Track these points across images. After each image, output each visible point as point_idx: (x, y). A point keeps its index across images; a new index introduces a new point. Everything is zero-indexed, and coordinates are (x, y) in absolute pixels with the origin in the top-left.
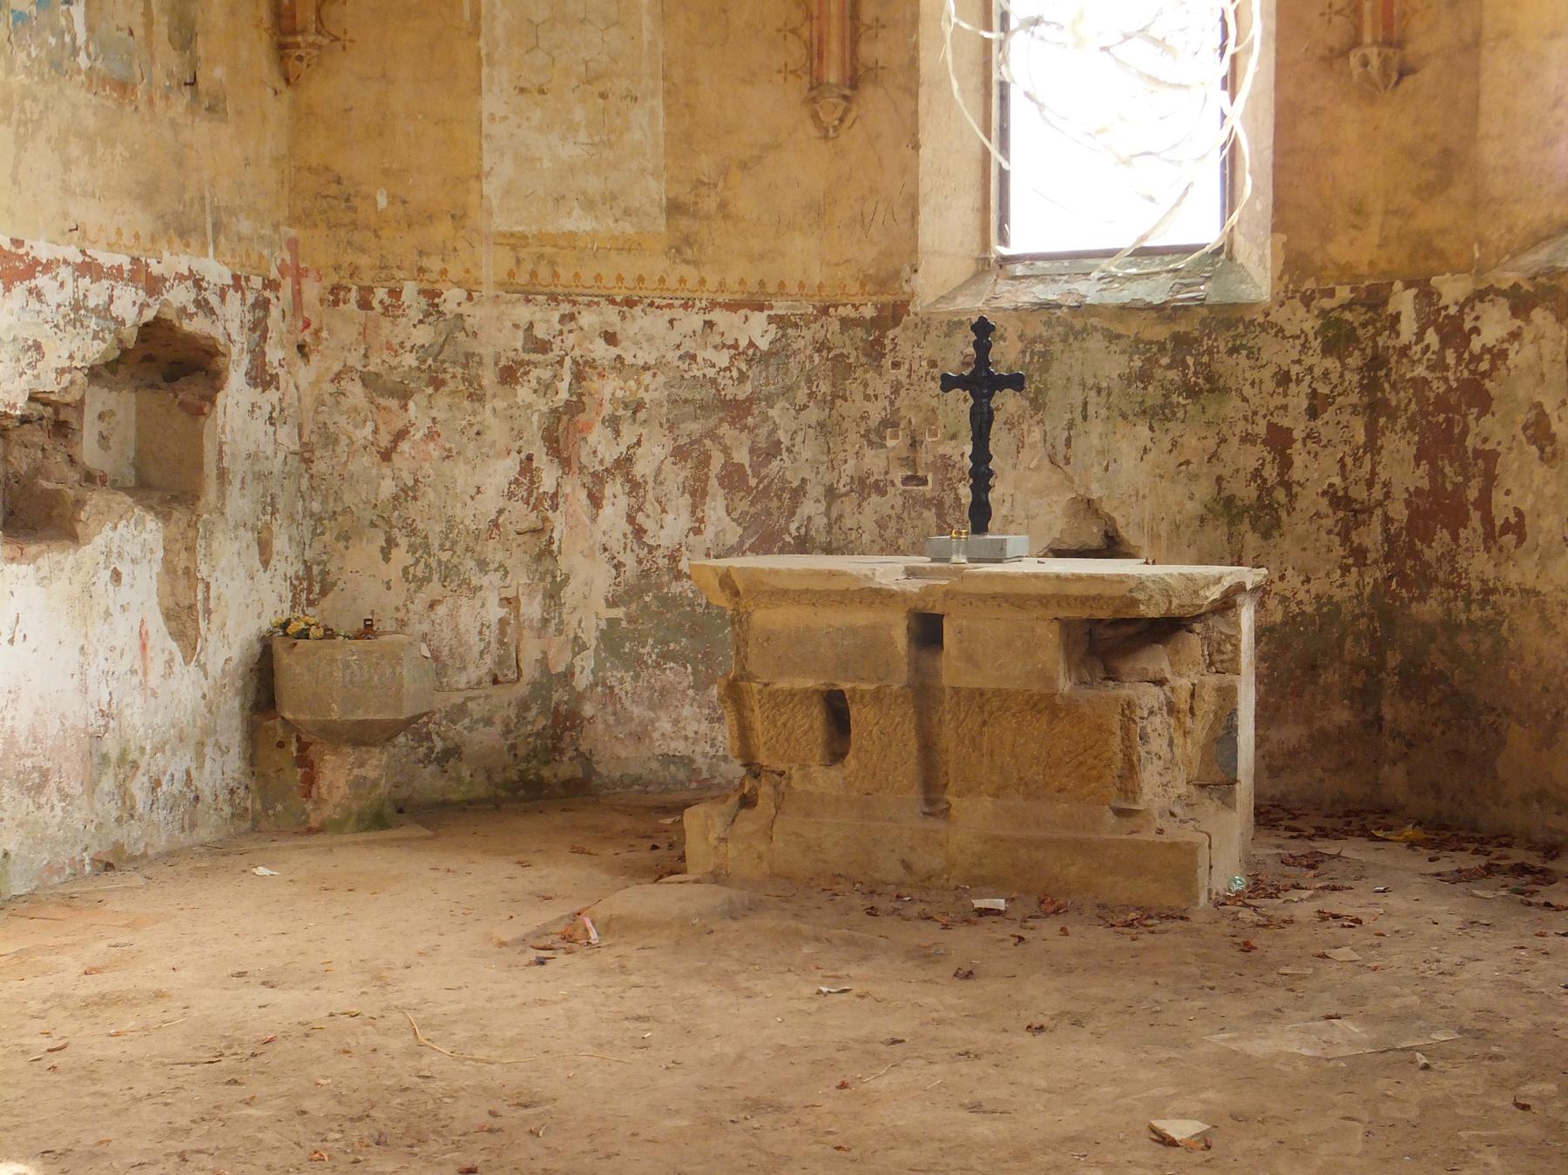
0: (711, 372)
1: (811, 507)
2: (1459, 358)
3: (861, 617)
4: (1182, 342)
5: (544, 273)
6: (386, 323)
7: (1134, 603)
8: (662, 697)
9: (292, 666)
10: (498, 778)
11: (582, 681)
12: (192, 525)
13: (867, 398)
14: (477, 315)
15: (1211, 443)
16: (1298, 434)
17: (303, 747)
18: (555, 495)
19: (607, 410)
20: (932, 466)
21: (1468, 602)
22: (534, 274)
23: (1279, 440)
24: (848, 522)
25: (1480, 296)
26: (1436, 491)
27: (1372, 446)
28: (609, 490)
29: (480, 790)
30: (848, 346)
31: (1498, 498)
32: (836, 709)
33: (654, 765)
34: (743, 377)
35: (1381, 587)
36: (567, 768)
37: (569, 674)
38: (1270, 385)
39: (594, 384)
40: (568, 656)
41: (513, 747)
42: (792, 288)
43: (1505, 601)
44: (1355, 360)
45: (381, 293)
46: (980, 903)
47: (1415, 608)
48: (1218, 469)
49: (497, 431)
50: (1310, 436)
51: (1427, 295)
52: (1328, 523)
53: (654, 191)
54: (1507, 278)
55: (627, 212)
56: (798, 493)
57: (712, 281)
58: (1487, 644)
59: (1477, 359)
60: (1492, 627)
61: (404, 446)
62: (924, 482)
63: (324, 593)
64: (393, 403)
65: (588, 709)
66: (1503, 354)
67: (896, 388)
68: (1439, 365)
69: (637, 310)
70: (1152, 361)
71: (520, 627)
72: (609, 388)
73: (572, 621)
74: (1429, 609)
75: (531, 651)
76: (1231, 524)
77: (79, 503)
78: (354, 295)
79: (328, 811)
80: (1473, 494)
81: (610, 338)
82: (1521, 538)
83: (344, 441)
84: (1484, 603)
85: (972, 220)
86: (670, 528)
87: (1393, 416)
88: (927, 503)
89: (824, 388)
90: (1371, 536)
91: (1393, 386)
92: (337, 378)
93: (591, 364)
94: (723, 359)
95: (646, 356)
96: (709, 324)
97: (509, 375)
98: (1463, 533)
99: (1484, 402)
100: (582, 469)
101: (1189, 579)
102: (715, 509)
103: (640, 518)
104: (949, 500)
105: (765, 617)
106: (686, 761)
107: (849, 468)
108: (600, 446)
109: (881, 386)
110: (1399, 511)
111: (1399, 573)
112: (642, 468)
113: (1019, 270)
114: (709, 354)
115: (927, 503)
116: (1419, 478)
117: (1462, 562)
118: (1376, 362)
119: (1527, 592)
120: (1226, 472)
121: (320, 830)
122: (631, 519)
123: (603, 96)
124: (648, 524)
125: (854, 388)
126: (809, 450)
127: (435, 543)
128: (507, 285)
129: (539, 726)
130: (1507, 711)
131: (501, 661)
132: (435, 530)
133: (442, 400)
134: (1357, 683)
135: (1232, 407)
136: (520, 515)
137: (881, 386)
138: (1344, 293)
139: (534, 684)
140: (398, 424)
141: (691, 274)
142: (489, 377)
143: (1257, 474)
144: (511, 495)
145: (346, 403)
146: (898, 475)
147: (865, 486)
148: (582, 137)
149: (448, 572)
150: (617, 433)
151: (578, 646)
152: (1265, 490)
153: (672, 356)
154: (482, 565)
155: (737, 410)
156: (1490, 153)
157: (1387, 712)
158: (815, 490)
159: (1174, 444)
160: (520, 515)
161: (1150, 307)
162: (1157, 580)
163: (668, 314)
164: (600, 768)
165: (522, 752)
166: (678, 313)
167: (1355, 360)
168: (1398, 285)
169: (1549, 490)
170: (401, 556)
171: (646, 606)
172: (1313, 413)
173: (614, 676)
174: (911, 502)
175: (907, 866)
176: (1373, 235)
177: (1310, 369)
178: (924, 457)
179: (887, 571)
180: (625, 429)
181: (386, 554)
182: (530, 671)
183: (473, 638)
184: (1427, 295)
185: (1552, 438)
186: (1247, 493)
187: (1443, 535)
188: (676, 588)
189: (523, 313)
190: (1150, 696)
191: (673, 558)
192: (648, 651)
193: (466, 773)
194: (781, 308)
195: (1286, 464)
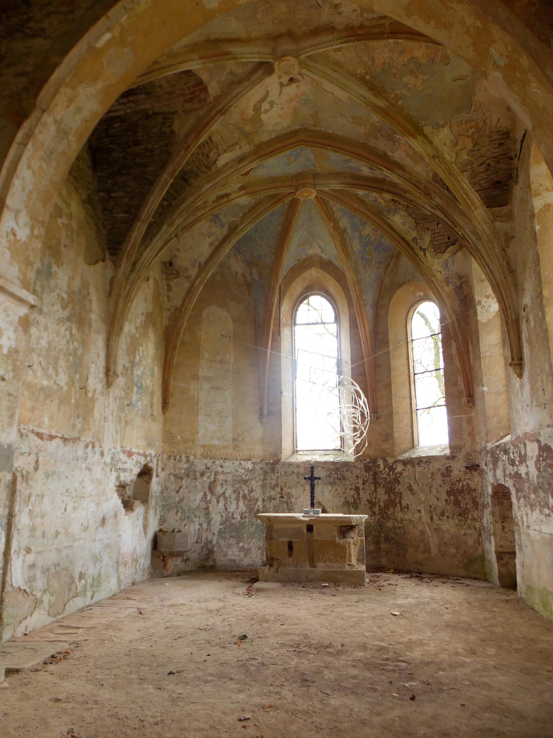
0: (240, 474)
1: (260, 503)
2: (393, 474)
3: (297, 526)
4: (337, 469)
5: (209, 453)
6: (179, 463)
7: (351, 522)
8: (230, 546)
9: (164, 540)
10: (197, 565)
12: (147, 507)
13: (271, 480)
14: (197, 462)
15: (344, 490)
16: (361, 488)
17: (164, 557)
18: (210, 501)
19: (221, 482)
20: (286, 494)
21: (398, 523)
22: (207, 453)
23: (357, 489)
24: (267, 507)
27: (375, 490)
28: (220, 500)
29: (193, 568)
31: (403, 501)
32: (290, 546)
33: (228, 562)
34: (246, 475)
35: (379, 520)
36: (210, 563)
37: (211, 541)
38: (355, 478)
39: (218, 476)
40: (211, 537)
41: (200, 558)
42: (256, 456)
43: (406, 522)
44: (371, 473)
45: (178, 457)
46: (324, 585)
47: (387, 524)
48: (345, 495)
49: (199, 487)
50: (363, 489)
51: (385, 461)
52: (368, 506)
53: (230, 436)
55: (225, 440)
56: (257, 500)
57: (241, 454)
58: (402, 531)
59: (397, 474)
61: (181, 490)
62: (284, 498)
63: (164, 523)
64: (179, 480)
65: (215, 549)
66: (402, 473)
67: (278, 477)
68: (388, 475)
69: (227, 461)
70: (331, 473)
71: (202, 530)
72: (221, 477)
73: (212, 528)
74: (390, 524)
75: (204, 536)
76: (348, 507)
77: (134, 503)
78: (173, 457)
79: (169, 572)
80: (397, 501)
81: (222, 467)
82: (408, 510)
83: (169, 489)
84: (401, 523)
85: (291, 443)
86: (232, 508)
87: (380, 485)
88: (285, 502)
89: (262, 477)
90: (376, 509)
91: (379, 479)
92: (169, 475)
93: (218, 472)
94: (243, 471)
95: (228, 470)
96: (240, 464)
97: (202, 474)
98: (396, 508)
99: (399, 483)
100: (216, 495)
101: (360, 517)
102: (241, 503)
103: (227, 506)
104: (289, 502)
107: (268, 494)
108: (219, 490)
109: (274, 477)
110: (382, 504)
111: (383, 517)
112: (227, 495)
113: (301, 453)
114: (240, 470)
115: (285, 502)
116: (386, 497)
117: (396, 514)
118: (376, 473)
119: (411, 520)
120: (347, 496)
121: (167, 576)
122: (225, 506)
123: (221, 417)
124: (228, 507)
125: (268, 477)
126: (259, 491)
127: (186, 511)
128: (202, 455)
129: (205, 553)
130: (407, 545)
131: (198, 538)
132: (186, 508)
133: (189, 480)
134: (375, 540)
135: (348, 482)
136: (203, 505)
137: (274, 477)
138: (368, 460)
139: (204, 543)
140: (180, 485)
141: (237, 453)
142: (198, 475)
143: (353, 496)
144: (201, 501)
145: (170, 480)
146: (278, 496)
147: (271, 499)
148: (217, 425)
149: (189, 518)
150: (223, 487)
151: (214, 534)
152: (355, 499)
153: (233, 471)
154: (195, 516)
155: (245, 482)
156: (396, 435)
157: (382, 546)
158: (260, 499)
159: (336, 490)
160: (203, 505)
161: (330, 462)
162: (355, 517)
163: (232, 461)
164: (218, 563)
165: (202, 559)
166: (234, 461)
167: (371, 473)
168: (379, 459)
169: (413, 500)
170: (179, 514)
171: (227, 525)
172: (364, 484)
174: (281, 502)
175: (307, 578)
176: (373, 449)
177: (363, 475)
178: (284, 492)
179: (299, 516)
180: (224, 486)
181: (176, 513)
183: (193, 533)
184: (385, 461)
185: (413, 490)
186: (351, 500)
187: (391, 509)
188: (233, 521)
189: (205, 461)
190: (352, 541)
191: (233, 514)
192: (227, 535)
193: (190, 564)
194: (254, 460)
195: (359, 494)
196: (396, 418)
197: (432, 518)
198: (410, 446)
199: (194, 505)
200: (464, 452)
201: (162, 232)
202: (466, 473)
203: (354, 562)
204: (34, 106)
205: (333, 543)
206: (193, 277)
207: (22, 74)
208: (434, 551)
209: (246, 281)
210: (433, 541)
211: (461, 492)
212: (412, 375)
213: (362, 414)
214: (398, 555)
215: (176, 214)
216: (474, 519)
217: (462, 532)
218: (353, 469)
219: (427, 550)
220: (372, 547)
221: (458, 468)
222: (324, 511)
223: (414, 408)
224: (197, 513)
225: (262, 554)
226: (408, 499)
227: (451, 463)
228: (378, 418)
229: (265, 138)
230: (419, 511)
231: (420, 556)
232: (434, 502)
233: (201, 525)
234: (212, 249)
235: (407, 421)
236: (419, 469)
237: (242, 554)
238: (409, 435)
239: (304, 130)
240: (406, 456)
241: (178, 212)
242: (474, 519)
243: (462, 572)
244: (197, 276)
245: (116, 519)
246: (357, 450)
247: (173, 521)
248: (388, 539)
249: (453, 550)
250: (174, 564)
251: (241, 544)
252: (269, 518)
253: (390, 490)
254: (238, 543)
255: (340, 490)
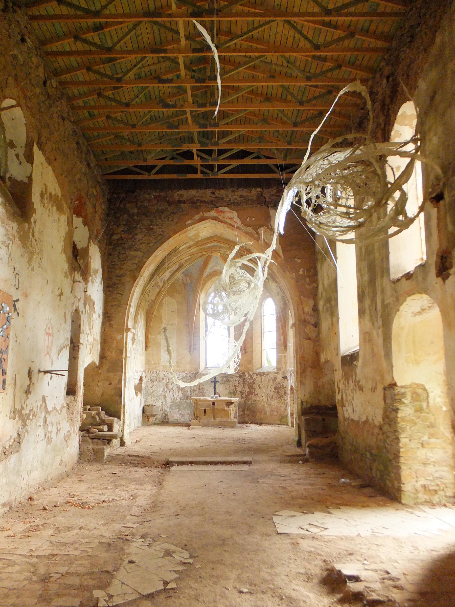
1: (189, 393)
3: (208, 403)
4: (226, 377)
8: (175, 413)
11: (168, 411)
14: (160, 373)
23: (235, 386)
25: (254, 374)
26: (250, 391)
27: (244, 387)
30: (192, 376)
36: (166, 420)
39: (170, 380)
43: (257, 401)
49: (162, 385)
51: (249, 373)
54: (256, 372)
56: (187, 391)
60: (255, 404)
68: (250, 380)
74: (250, 402)
75: (164, 408)
79: (150, 423)
90: (244, 396)
97: (163, 379)
99: (254, 383)
105: (199, 403)
106: (177, 419)
108: (170, 386)
110: (247, 393)
112: (174, 389)
116: (248, 390)
118: (244, 379)
132: (156, 395)
135: (231, 383)
138: (241, 372)
142: (161, 379)
149: (157, 399)
152: (234, 391)
156: (254, 361)
158: (189, 391)
170: (153, 398)
173: (171, 410)
174: (199, 392)
178: (201, 387)
179: (209, 399)
182: (163, 410)
184: (249, 373)
186: (232, 391)
189: (164, 373)
190: (232, 409)
195: (236, 388)
196: (254, 353)
197: (268, 399)
198: (260, 366)
199: (159, 394)
200: (282, 370)
201: (154, 278)
202: (282, 380)
203: (232, 417)
204: (139, 275)
205: (223, 410)
206: (161, 286)
207: (135, 263)
208: (268, 414)
209: (183, 283)
210: (268, 409)
211: (280, 388)
212: (263, 332)
213: (238, 355)
214: (253, 416)
215: (161, 270)
216: (284, 400)
217: (280, 405)
218: (234, 377)
219: (265, 414)
220: (241, 413)
221: (279, 377)
222: (220, 396)
223: (263, 348)
224: (161, 397)
225: (190, 416)
226: (258, 391)
227: (277, 375)
228: (246, 353)
229: (200, 239)
230: (263, 396)
231: (262, 416)
232: (269, 392)
233: (162, 403)
234: (170, 274)
235: (259, 355)
236: (263, 377)
237: (180, 416)
238: (260, 361)
239: (216, 236)
240: (258, 371)
241: (162, 269)
242: (284, 400)
243: (279, 422)
244: (163, 286)
245: (362, 391)
246: (236, 369)
247: (150, 401)
248: (248, 409)
249: (276, 413)
250: (152, 419)
251: (180, 412)
252: (196, 400)
253: (250, 387)
254: (179, 411)
255: (227, 386)
